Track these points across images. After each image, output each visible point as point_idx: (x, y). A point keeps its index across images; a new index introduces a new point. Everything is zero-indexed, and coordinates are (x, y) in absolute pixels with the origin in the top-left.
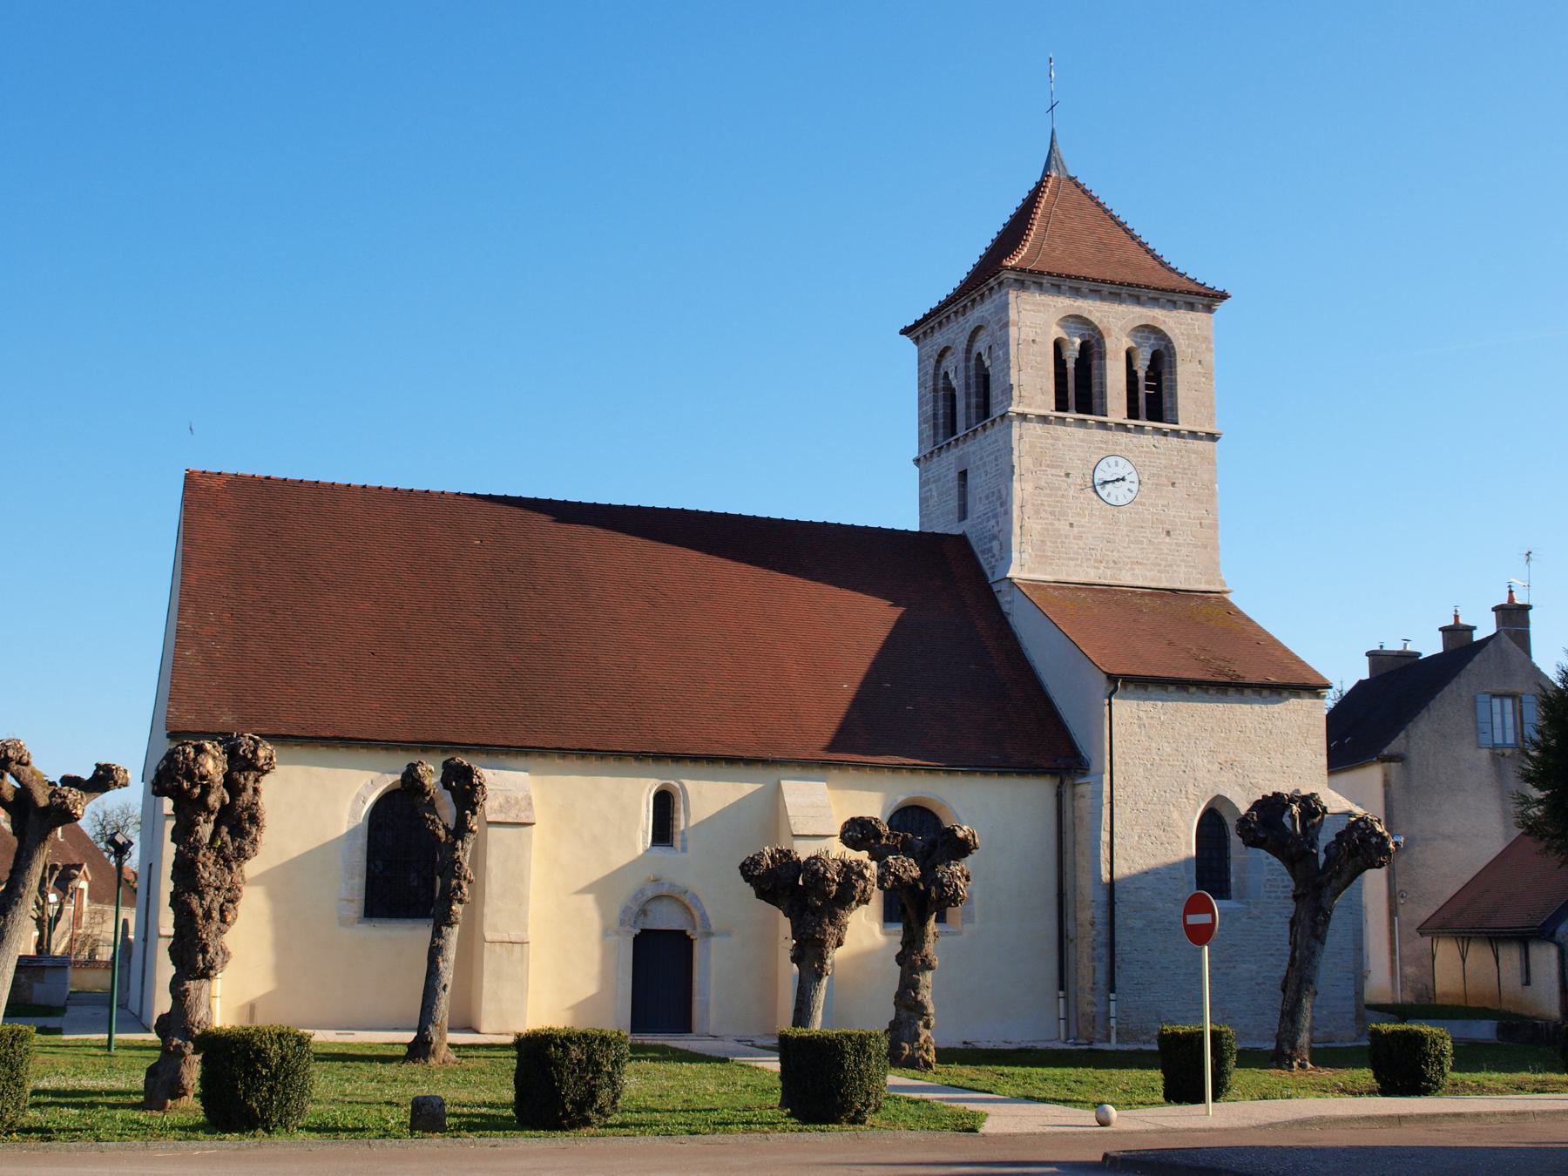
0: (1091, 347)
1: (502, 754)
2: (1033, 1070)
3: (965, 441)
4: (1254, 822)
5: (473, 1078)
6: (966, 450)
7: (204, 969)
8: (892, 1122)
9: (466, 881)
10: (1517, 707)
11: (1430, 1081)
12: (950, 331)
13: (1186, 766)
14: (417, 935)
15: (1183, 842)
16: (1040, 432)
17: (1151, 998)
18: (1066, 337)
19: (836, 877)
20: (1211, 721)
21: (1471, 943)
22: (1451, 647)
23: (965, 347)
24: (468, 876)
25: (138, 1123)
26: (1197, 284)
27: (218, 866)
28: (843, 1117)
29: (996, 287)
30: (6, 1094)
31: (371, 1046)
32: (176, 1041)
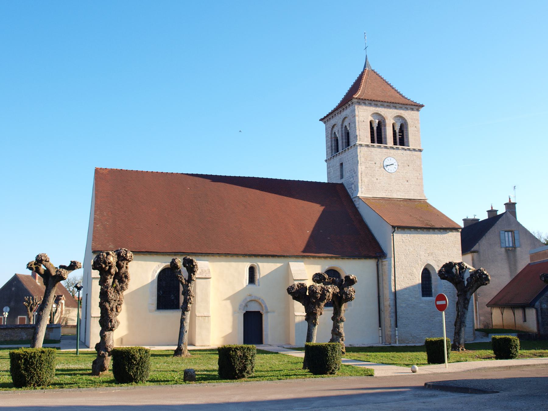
0: (381, 123)
1: (200, 256)
2: (377, 353)
3: (342, 154)
4: (444, 272)
5: (197, 361)
6: (342, 156)
7: (111, 328)
8: (343, 373)
9: (192, 297)
10: (513, 235)
11: (513, 354)
12: (336, 119)
13: (417, 255)
14: (176, 315)
15: (417, 279)
16: (366, 150)
17: (409, 329)
18: (373, 120)
19: (320, 292)
20: (425, 240)
21: (494, 308)
22: (491, 217)
23: (341, 124)
24: (193, 295)
25: (91, 380)
26: (414, 102)
27: (115, 293)
28: (328, 372)
29: (351, 104)
30: (47, 372)
31: (161, 351)
32: (102, 352)
